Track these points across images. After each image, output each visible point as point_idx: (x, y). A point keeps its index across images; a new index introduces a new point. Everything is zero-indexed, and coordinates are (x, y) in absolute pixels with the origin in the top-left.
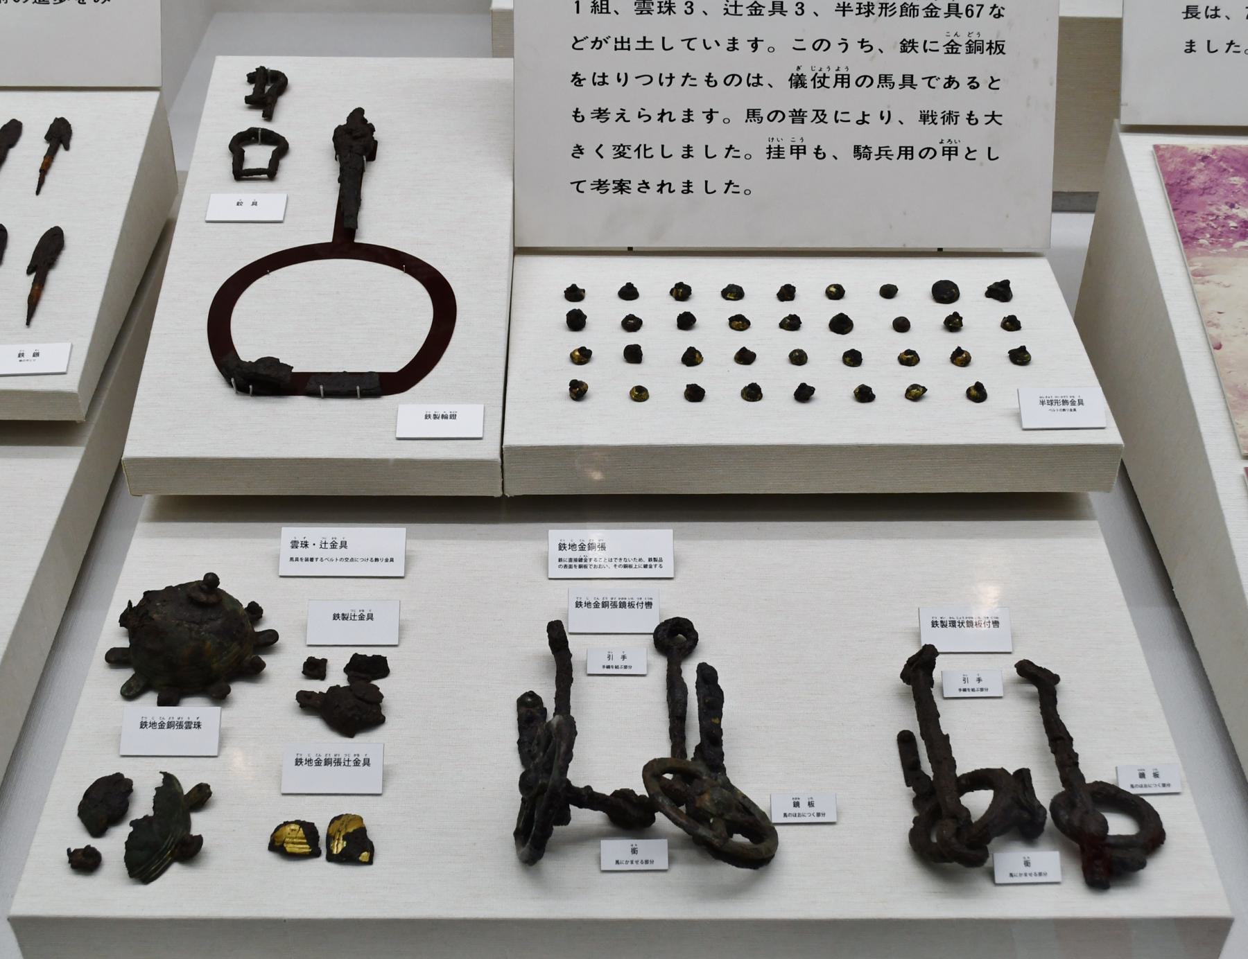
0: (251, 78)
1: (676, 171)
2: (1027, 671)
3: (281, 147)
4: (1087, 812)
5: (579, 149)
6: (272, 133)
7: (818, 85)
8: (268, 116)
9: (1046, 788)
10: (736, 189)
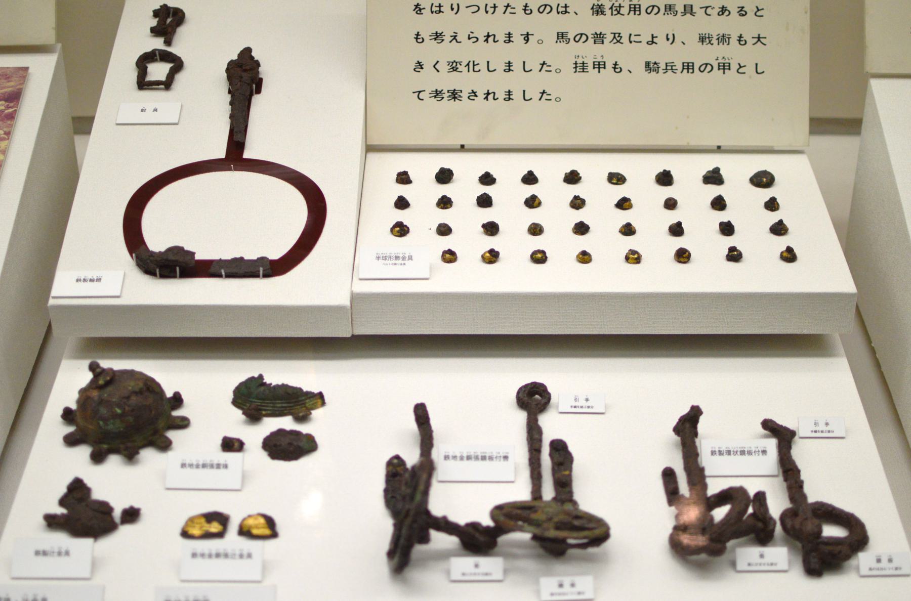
0: (156, 14)
1: (499, 83)
2: (771, 427)
3: (177, 65)
4: (806, 519)
5: (420, 65)
6: (171, 53)
7: (615, 13)
8: (168, 43)
9: (777, 505)
10: (549, 97)
